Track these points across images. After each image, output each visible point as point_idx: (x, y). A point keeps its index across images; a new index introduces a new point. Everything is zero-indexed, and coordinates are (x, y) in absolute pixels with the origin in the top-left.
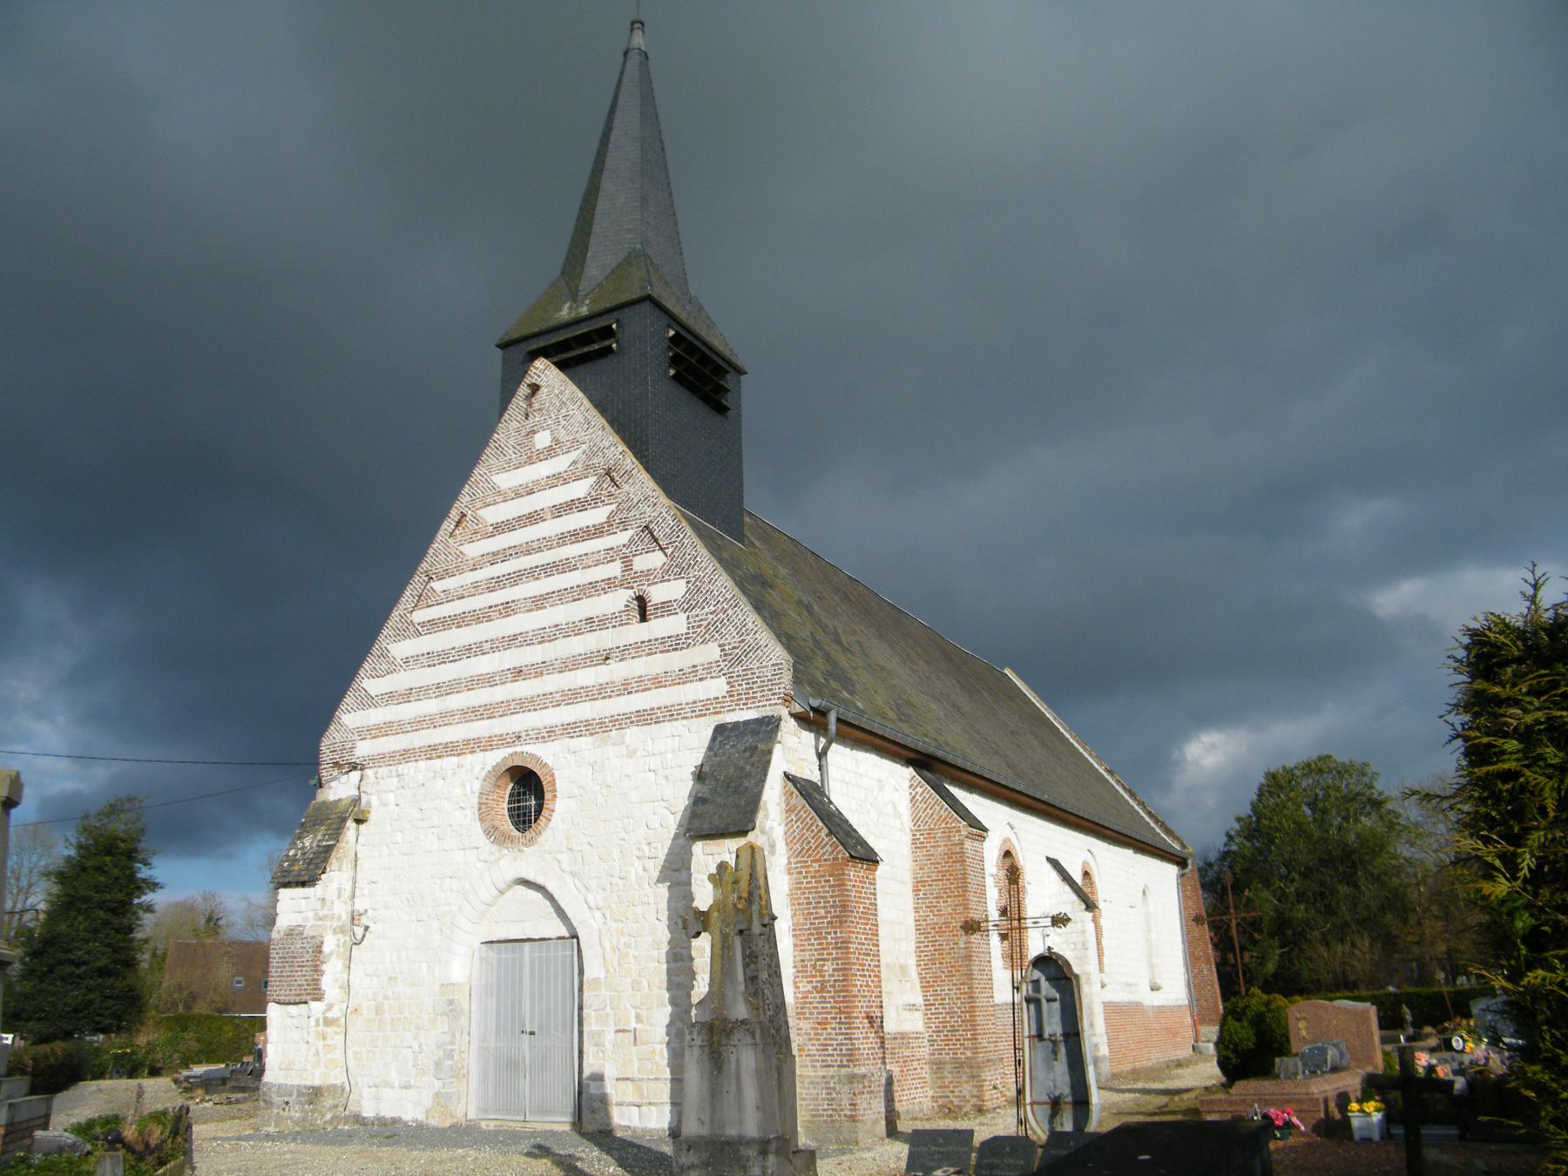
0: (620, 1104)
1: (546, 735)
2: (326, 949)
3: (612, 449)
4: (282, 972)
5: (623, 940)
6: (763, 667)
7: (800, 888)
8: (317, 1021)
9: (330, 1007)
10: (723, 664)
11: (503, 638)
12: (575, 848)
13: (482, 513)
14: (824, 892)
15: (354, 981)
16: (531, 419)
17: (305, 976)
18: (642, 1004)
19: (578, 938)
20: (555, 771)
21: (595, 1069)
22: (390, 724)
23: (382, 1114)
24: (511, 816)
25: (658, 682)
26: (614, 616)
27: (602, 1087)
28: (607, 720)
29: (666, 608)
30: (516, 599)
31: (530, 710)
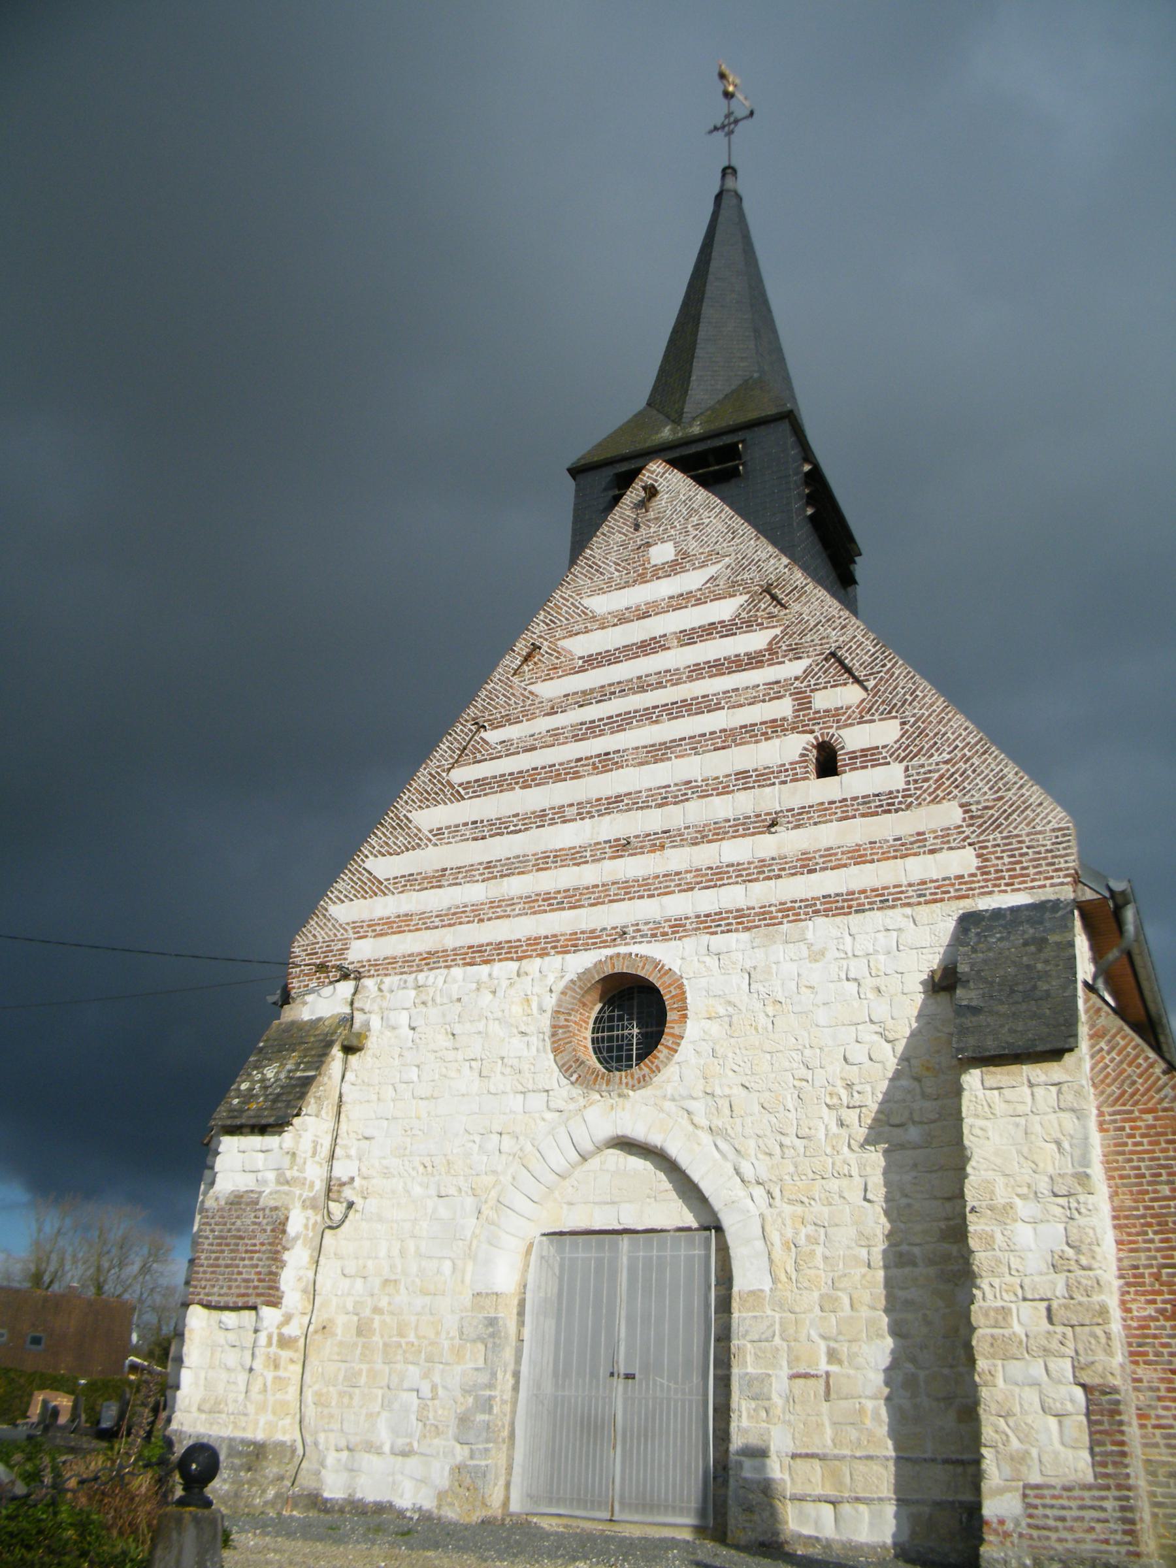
0: (796, 1498)
1: (670, 931)
2: (292, 1228)
3: (772, 561)
4: (217, 1259)
5: (803, 1231)
6: (1036, 833)
7: (1123, 1153)
8: (270, 1337)
9: (288, 1319)
10: (968, 831)
11: (598, 800)
12: (718, 1091)
13: (566, 644)
14: (1167, 1158)
15: (325, 1283)
16: (643, 530)
17: (256, 1266)
18: (840, 1333)
19: (719, 1229)
20: (685, 982)
21: (753, 1440)
22: (408, 916)
23: (359, 1495)
24: (597, 1051)
25: (859, 856)
26: (782, 769)
27: (762, 1468)
28: (773, 909)
29: (869, 757)
30: (621, 748)
31: (642, 897)
